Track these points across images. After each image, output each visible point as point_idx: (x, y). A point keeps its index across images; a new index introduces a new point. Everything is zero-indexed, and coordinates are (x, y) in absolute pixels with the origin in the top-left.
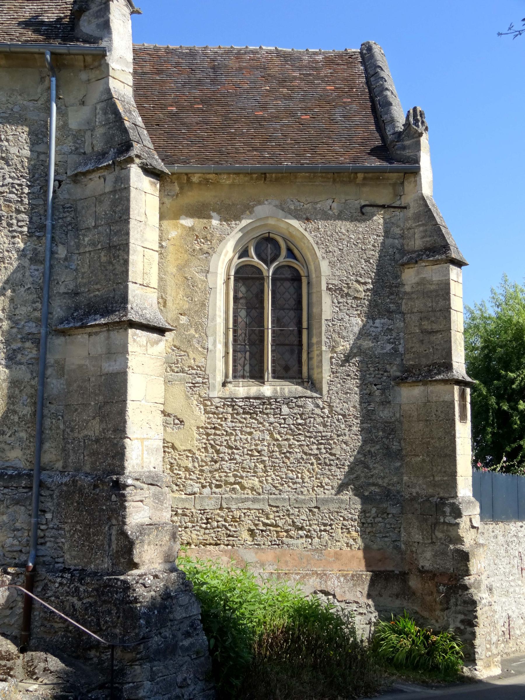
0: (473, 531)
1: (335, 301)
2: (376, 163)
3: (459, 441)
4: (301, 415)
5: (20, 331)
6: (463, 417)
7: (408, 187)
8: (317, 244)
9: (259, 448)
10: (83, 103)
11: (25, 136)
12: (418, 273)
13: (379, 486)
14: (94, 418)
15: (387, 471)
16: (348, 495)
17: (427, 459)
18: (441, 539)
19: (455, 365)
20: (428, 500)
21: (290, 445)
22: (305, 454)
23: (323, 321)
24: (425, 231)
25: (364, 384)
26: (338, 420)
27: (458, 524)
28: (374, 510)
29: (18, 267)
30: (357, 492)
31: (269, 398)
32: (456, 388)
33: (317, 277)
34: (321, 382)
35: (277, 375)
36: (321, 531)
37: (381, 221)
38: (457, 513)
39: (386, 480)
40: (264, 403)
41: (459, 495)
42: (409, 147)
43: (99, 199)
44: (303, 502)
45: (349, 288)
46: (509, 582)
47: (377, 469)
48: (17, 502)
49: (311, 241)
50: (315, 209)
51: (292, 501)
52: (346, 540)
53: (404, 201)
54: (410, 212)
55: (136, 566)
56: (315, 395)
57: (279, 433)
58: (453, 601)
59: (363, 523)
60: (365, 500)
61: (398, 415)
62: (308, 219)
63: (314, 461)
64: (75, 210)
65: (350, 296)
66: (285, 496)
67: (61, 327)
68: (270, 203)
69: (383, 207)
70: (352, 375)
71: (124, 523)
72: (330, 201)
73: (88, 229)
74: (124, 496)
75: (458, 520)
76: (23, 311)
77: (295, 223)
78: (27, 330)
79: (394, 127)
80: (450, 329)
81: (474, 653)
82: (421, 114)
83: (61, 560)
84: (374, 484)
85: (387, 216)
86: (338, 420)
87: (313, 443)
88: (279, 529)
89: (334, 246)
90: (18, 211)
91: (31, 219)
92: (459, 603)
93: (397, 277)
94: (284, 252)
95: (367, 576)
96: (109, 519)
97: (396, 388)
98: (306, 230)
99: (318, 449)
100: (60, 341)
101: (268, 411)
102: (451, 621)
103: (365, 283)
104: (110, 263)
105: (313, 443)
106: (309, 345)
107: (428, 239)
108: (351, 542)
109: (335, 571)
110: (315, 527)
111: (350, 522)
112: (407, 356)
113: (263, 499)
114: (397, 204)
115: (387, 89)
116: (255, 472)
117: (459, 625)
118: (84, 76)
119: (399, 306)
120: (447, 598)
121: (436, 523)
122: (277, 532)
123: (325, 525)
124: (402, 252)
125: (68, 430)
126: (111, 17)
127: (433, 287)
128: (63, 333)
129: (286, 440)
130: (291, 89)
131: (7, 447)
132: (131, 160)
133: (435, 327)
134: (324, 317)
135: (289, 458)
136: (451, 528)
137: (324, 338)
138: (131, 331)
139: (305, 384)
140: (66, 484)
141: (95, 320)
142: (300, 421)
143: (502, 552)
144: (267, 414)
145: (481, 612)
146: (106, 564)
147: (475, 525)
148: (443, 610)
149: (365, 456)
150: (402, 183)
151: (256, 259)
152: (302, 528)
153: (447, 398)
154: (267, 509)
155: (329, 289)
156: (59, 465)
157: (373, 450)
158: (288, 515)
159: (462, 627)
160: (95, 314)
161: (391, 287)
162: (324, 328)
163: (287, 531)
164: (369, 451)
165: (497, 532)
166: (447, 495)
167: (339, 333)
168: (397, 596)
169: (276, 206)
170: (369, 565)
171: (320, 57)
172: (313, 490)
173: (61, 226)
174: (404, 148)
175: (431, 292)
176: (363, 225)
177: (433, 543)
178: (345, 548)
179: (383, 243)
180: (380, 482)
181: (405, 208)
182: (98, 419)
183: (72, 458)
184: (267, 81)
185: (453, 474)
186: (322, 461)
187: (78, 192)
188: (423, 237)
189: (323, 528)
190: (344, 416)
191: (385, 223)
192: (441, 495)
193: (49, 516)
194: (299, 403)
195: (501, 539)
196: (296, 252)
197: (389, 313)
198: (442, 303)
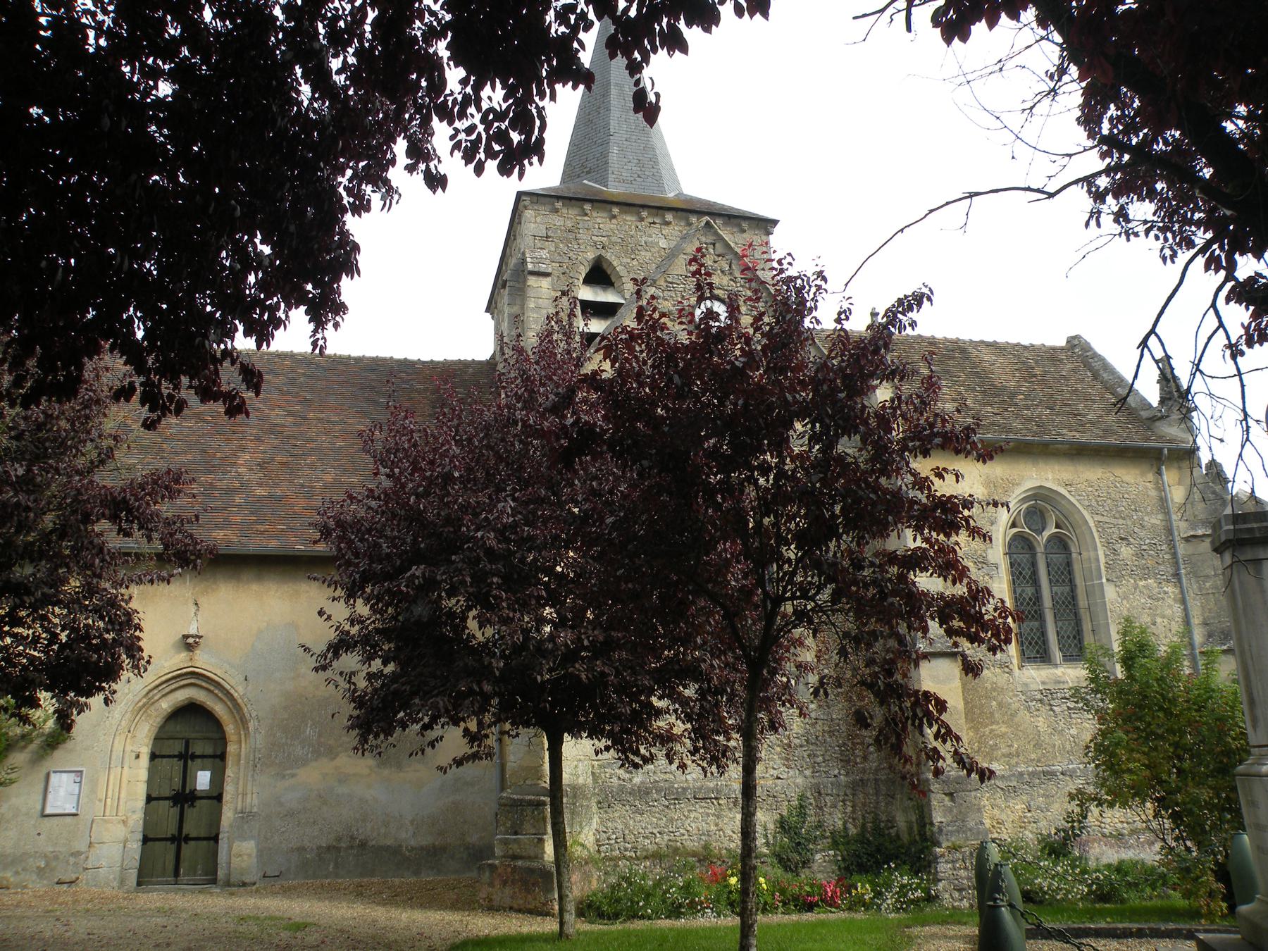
73: (1207, 576)
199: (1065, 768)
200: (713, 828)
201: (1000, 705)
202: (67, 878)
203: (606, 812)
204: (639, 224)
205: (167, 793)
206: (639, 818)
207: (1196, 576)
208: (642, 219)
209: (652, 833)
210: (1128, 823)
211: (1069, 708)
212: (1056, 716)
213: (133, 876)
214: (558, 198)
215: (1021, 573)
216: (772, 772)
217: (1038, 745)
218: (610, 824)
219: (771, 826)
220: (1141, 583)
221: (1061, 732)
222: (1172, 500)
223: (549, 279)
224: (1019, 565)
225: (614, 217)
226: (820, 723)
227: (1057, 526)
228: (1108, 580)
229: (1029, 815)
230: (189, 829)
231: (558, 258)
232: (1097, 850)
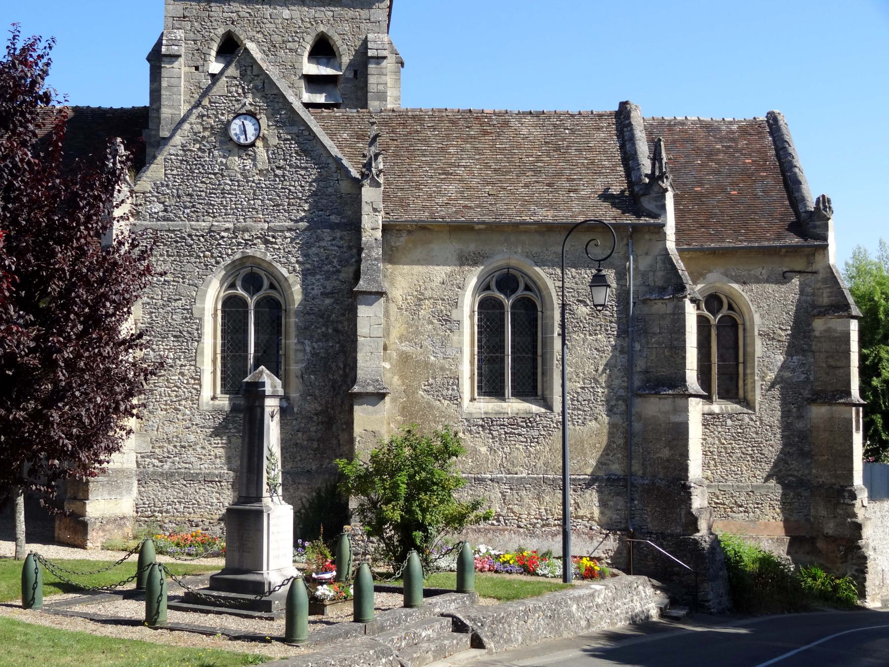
0: (863, 509)
1: (765, 343)
2: (795, 240)
4: (740, 426)
5: (615, 394)
6: (858, 429)
7: (818, 257)
8: (751, 301)
9: (711, 449)
10: (647, 254)
11: (613, 275)
12: (825, 323)
13: (795, 477)
14: (665, 447)
15: (801, 466)
16: (772, 483)
17: (831, 458)
18: (841, 514)
20: (831, 487)
21: (732, 448)
22: (744, 454)
23: (756, 359)
24: (831, 292)
25: (784, 403)
26: (766, 430)
27: (854, 505)
28: (792, 494)
29: (612, 356)
30: (780, 481)
31: (718, 414)
32: (854, 409)
33: (751, 325)
34: (754, 402)
35: (721, 397)
36: (755, 508)
37: (798, 283)
38: (854, 497)
39: (800, 473)
40: (714, 418)
41: (855, 484)
42: (819, 227)
43: (662, 317)
44: (742, 487)
45: (774, 333)
46: (883, 545)
47: (794, 465)
48: (618, 494)
49: (747, 299)
50: (750, 275)
51: (735, 487)
52: (772, 514)
53: (814, 268)
54: (820, 276)
55: (698, 531)
56: (750, 412)
57: (725, 439)
58: (850, 556)
59: (784, 503)
60: (786, 486)
61: (809, 426)
62: (745, 283)
63: (749, 459)
64: (644, 321)
65: (775, 339)
66: (729, 483)
67: (640, 392)
68: (717, 272)
69: (800, 272)
70: (777, 397)
71: (691, 508)
72: (760, 269)
73: (655, 334)
74: (690, 493)
75: (854, 502)
76: (617, 382)
77: (736, 286)
78: (619, 394)
79: (805, 206)
81: (865, 591)
82: (829, 201)
83: (645, 527)
84: (791, 475)
85: (802, 279)
86: (766, 430)
87: (749, 446)
88: (725, 506)
89: (763, 302)
90: (611, 322)
91: (618, 326)
92: (854, 557)
93: (809, 325)
94: (726, 306)
95: (787, 539)
96: (680, 505)
97: (808, 407)
98: (743, 291)
99: (752, 450)
100: (638, 401)
101: (717, 423)
102: (848, 570)
103: (786, 330)
104: (672, 356)
105: (749, 446)
106: (745, 375)
107: (833, 298)
108: (776, 516)
109: (765, 536)
110: (751, 505)
111: (775, 502)
112: (816, 384)
113: (715, 486)
114: (810, 270)
115: (795, 166)
116: (709, 467)
117: (854, 572)
118: (647, 237)
119: (810, 346)
120: (846, 555)
121: (838, 503)
122: (724, 508)
123: (758, 504)
124: (814, 306)
125: (646, 453)
126: (666, 202)
127: (837, 335)
128: (641, 396)
129: (731, 444)
130: (718, 162)
131: (610, 463)
132: (686, 297)
133: (839, 364)
134: (756, 355)
135: (731, 457)
136: (848, 507)
137: (756, 371)
138: (690, 399)
139: (742, 403)
140: (647, 484)
141: (665, 391)
142: (739, 431)
143: (879, 523)
144: (716, 426)
145: (870, 564)
146: (679, 530)
147: (865, 505)
148: (842, 563)
149: (785, 455)
150: (814, 254)
151: (706, 312)
152: (741, 506)
153: (847, 416)
154: (718, 492)
155: (760, 335)
156: (640, 473)
157: (791, 451)
158: (732, 497)
159: (856, 574)
160: (663, 387)
161: (805, 332)
162: (756, 363)
163: (731, 508)
164: (788, 452)
165: (875, 508)
166: (846, 484)
167: (767, 367)
168: (808, 553)
169: (722, 273)
170: (788, 532)
171: (735, 127)
172: (749, 479)
173: (637, 331)
174: (815, 227)
175: (835, 338)
176: (784, 286)
177: (835, 517)
178: (771, 520)
179: (799, 300)
180: (796, 473)
181: (816, 273)
182: (668, 448)
183: (649, 469)
184: (698, 155)
185: (851, 470)
186: (755, 459)
187: (646, 309)
188: (829, 297)
189: (756, 506)
190: (771, 427)
191: (801, 284)
192: (842, 484)
193: (636, 502)
194: (739, 418)
195: (878, 514)
196: (734, 305)
197: (803, 352)
198: (844, 347)
200: (215, 501)
203: (143, 487)
206: (165, 491)
209: (173, 502)
210: (542, 520)
211: (506, 433)
218: (145, 494)
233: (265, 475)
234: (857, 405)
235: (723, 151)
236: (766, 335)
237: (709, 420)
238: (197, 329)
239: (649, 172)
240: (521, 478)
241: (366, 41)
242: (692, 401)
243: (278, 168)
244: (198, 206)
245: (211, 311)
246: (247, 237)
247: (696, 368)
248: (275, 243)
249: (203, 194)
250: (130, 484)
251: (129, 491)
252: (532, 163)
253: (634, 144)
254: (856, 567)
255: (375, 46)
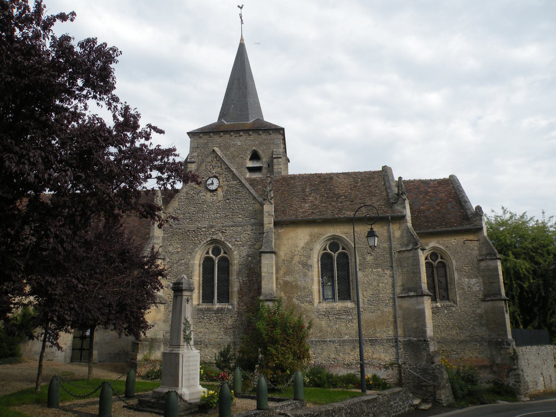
3: (506, 320)
9: (438, 324)
19: (502, 294)
23: (456, 281)
80: (499, 282)
84: (477, 335)
104: (414, 277)
117: (514, 382)
127: (491, 268)
130: (429, 196)
132: (418, 248)
138: (424, 297)
140: (407, 341)
152: (455, 351)
168: (490, 373)
199: (331, 339)
201: (307, 316)
202: (50, 359)
204: (230, 137)
205: (79, 336)
207: (401, 266)
208: (232, 136)
211: (336, 318)
212: (330, 320)
213: (68, 360)
214: (201, 133)
215: (326, 268)
216: (220, 336)
217: (321, 331)
219: (217, 354)
220: (374, 270)
221: (331, 327)
222: (394, 236)
223: (195, 164)
224: (326, 265)
225: (221, 136)
226: (238, 321)
227: (343, 249)
228: (359, 270)
229: (314, 355)
230: (84, 347)
231: (201, 155)
232: (338, 369)
233: (182, 333)
234: (505, 300)
235: (432, 192)
236: (459, 270)
237: (435, 311)
238: (191, 273)
239: (397, 192)
240: (344, 340)
241: (273, 152)
242: (426, 298)
243: (228, 199)
244: (192, 218)
245: (317, 290)
246: (213, 230)
247: (426, 282)
248: (226, 233)
249: (195, 212)
250: (160, 346)
251: (159, 349)
252: (344, 193)
253: (389, 183)
254: (514, 380)
255: (276, 153)
